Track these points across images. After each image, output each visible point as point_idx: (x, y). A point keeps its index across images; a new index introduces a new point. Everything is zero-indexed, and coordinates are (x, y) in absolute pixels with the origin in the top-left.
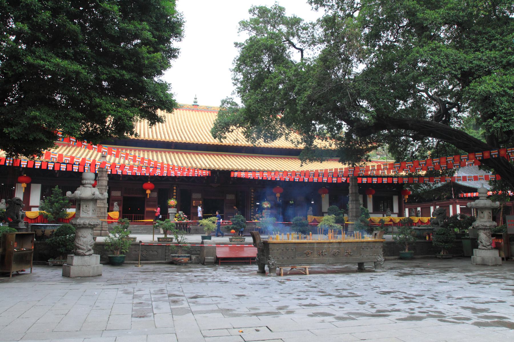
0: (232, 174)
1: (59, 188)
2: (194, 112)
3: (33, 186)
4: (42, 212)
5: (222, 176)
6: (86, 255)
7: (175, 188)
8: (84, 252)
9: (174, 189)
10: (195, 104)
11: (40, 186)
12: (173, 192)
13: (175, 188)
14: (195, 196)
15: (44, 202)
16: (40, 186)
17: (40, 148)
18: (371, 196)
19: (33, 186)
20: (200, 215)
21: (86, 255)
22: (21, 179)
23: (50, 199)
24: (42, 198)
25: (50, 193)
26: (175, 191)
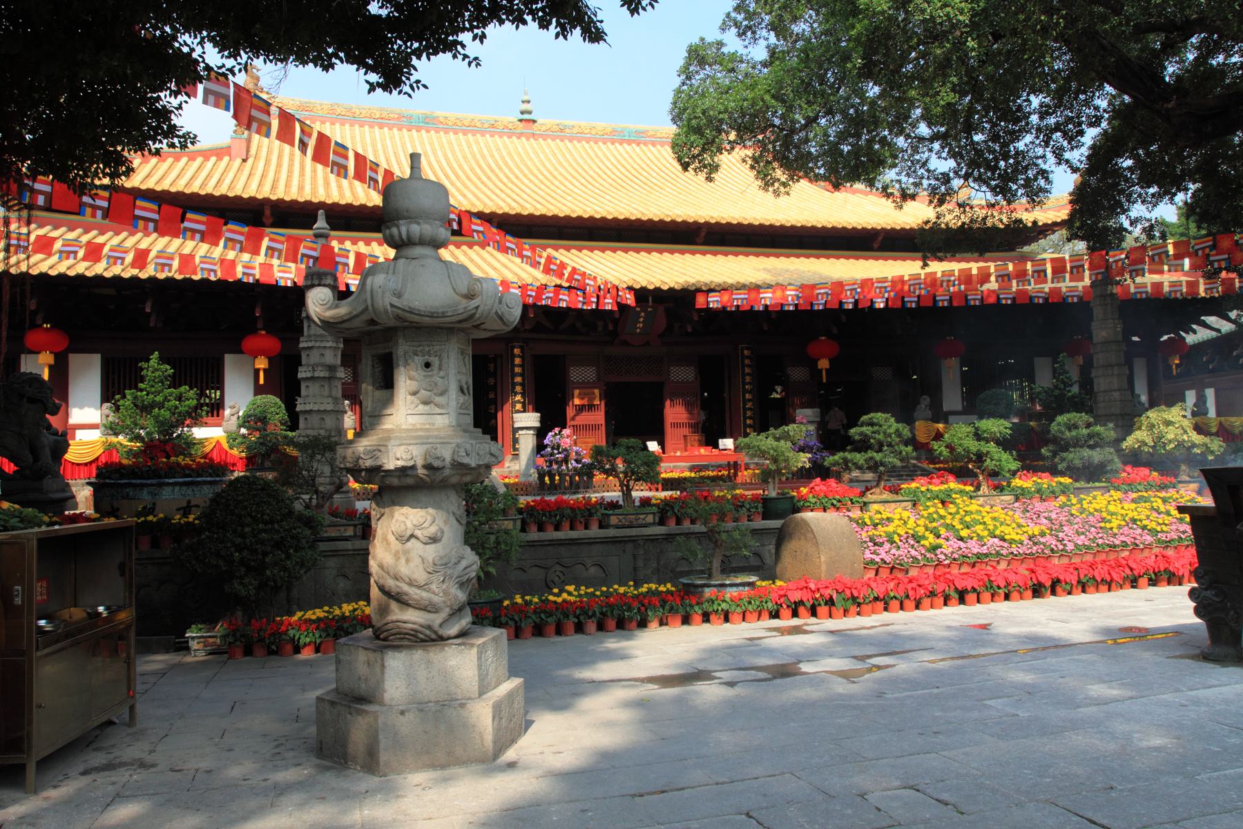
0: (700, 301)
1: (162, 360)
2: (523, 139)
3: (75, 360)
4: (114, 439)
5: (675, 304)
6: (442, 639)
7: (517, 351)
8: (436, 619)
9: (513, 356)
10: (526, 116)
11: (96, 360)
12: (513, 366)
13: (517, 351)
14: (577, 374)
15: (117, 409)
16: (96, 360)
17: (172, 47)
18: (954, 362)
19: (75, 360)
20: (1144, 398)
21: (442, 639)
22: (31, 338)
23: (136, 398)
24: (106, 398)
25: (134, 379)
26: (517, 361)
